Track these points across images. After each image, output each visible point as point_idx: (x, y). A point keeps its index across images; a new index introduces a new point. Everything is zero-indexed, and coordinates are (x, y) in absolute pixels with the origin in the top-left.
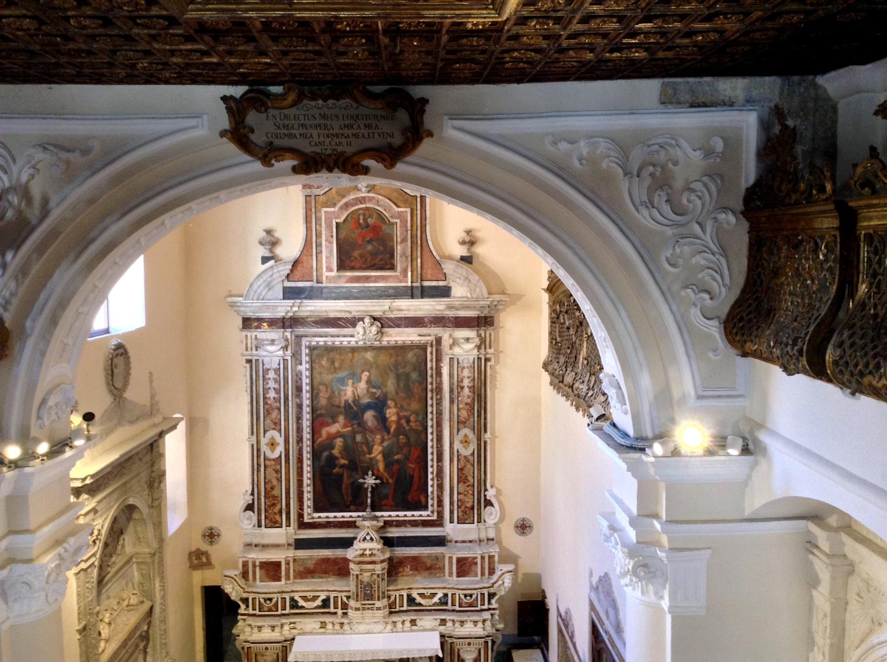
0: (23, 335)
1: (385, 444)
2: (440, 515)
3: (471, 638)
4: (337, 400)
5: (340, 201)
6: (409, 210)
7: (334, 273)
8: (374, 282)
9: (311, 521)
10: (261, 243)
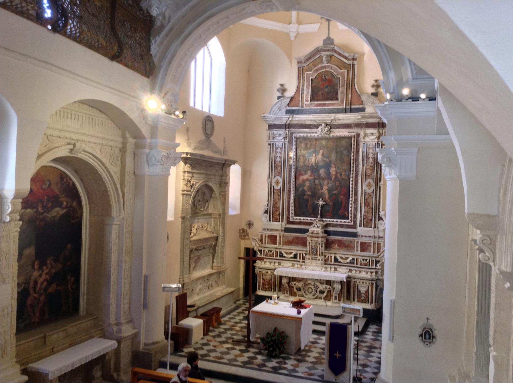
0: (160, 67)
2: (355, 222)
3: (364, 279)
5: (313, 69)
6: (346, 71)
7: (309, 102)
9: (293, 220)
10: (278, 90)
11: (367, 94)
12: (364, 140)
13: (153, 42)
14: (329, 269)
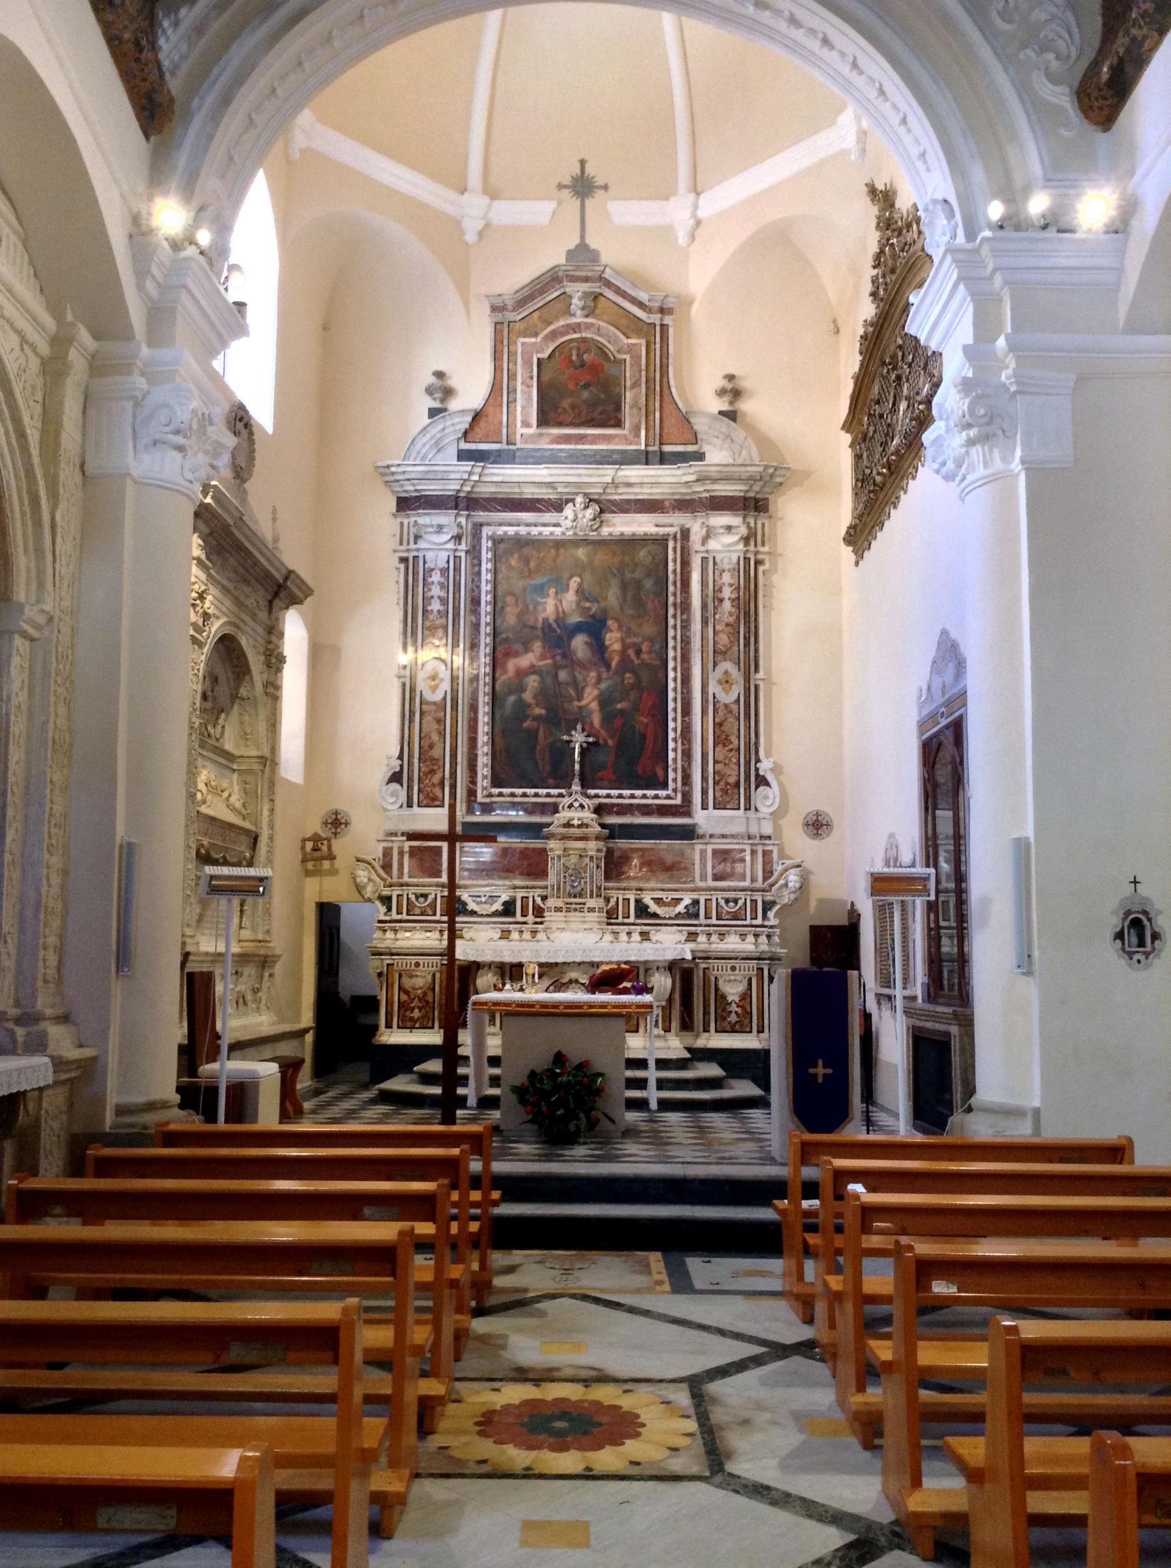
0: (188, 115)
1: (603, 686)
3: (736, 959)
4: (532, 619)
6: (643, 342)
7: (533, 430)
8: (592, 443)
9: (487, 800)
11: (707, 415)
12: (703, 549)
13: (166, 23)
14: (623, 937)
